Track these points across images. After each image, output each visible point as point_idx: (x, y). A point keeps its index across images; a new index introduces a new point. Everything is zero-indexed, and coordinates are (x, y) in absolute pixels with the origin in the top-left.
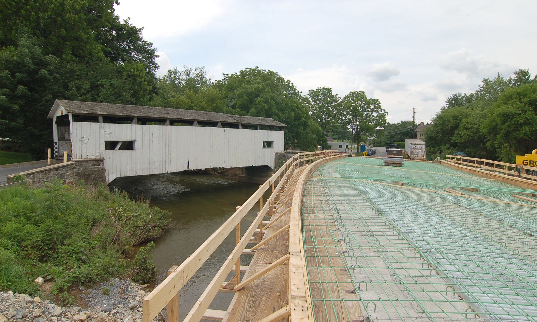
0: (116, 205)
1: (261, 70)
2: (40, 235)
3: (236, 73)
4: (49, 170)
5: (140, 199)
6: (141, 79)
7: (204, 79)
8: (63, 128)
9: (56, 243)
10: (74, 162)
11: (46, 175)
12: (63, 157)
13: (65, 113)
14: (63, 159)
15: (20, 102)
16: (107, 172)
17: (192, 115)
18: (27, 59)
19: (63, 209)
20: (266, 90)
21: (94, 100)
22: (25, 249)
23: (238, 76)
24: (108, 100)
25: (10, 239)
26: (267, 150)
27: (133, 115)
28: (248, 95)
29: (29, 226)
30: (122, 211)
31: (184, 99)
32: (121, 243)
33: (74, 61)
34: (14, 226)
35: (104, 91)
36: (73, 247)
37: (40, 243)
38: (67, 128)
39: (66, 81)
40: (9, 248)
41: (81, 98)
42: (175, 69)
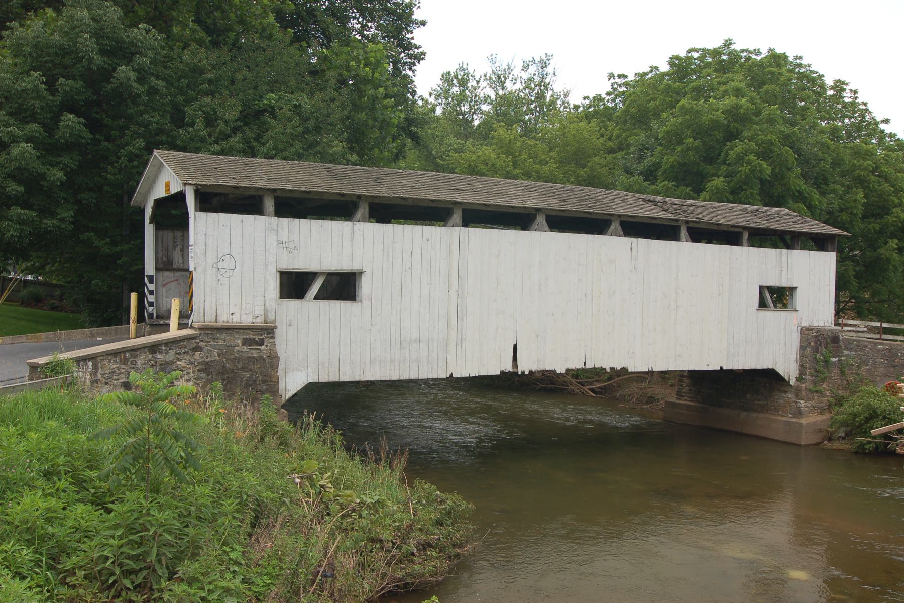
0: (313, 465)
1: (742, 51)
2: (112, 541)
3: (657, 68)
4: (134, 350)
5: (378, 452)
6: (376, 88)
7: (549, 95)
8: (168, 235)
9: (154, 571)
10: (198, 332)
11: (124, 364)
12: (169, 317)
13: (174, 190)
14: (169, 325)
15: (66, 160)
16: (281, 366)
17: (527, 194)
18: (86, 39)
19: (178, 463)
20: (765, 113)
21: (251, 152)
22: (68, 580)
23: (664, 75)
24: (286, 154)
25: (29, 543)
26: (774, 317)
27: (357, 192)
28: (700, 132)
29: (80, 508)
30: (330, 485)
31: (493, 156)
32: (340, 590)
33: (200, 43)
34: (42, 504)
35: (276, 128)
36: (203, 589)
37: (111, 567)
38: (179, 234)
39: (180, 98)
40: (25, 572)
41: (217, 148)
42: (461, 69)
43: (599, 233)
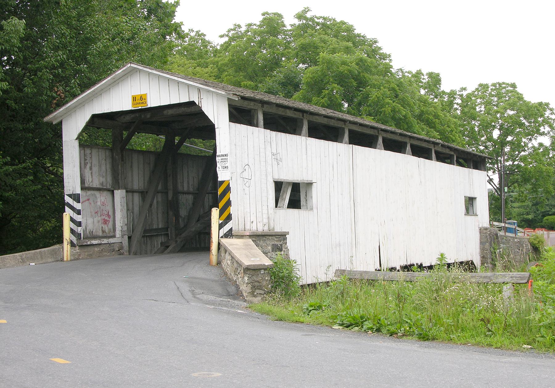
43: (400, 151)
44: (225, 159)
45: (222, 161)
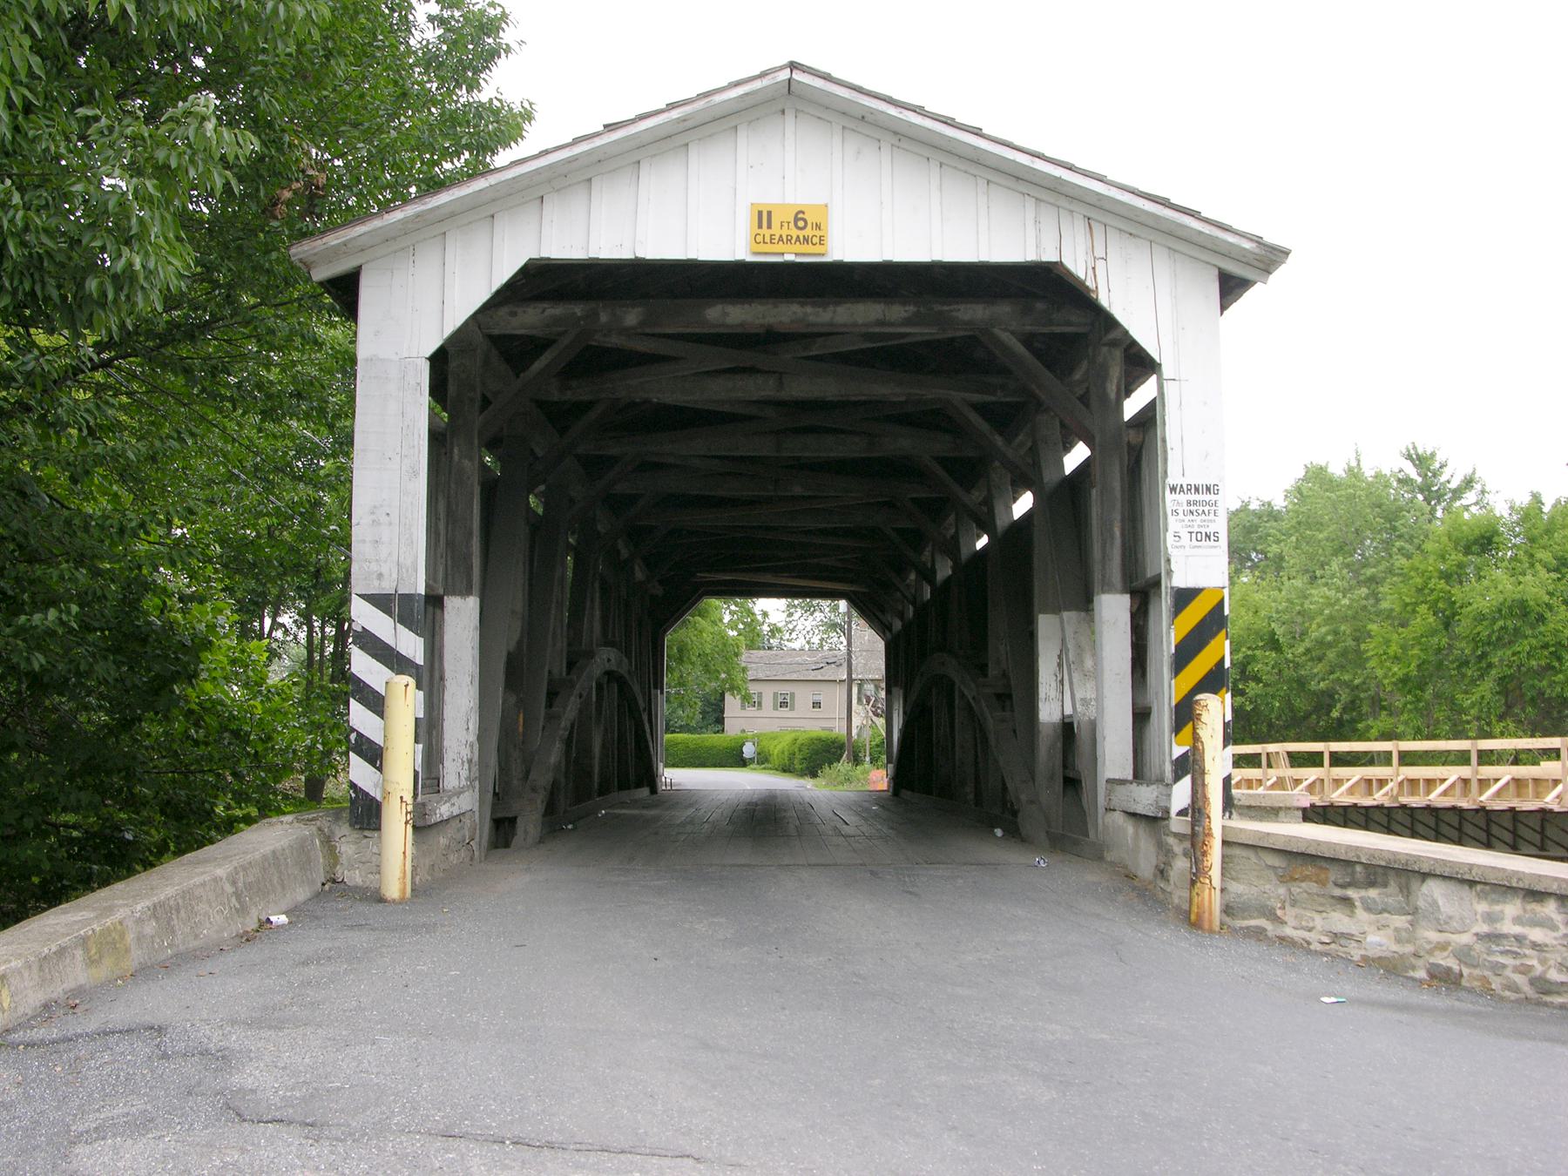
44: (1208, 503)
45: (1192, 508)
